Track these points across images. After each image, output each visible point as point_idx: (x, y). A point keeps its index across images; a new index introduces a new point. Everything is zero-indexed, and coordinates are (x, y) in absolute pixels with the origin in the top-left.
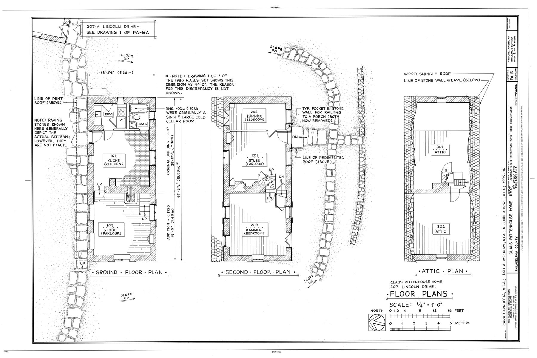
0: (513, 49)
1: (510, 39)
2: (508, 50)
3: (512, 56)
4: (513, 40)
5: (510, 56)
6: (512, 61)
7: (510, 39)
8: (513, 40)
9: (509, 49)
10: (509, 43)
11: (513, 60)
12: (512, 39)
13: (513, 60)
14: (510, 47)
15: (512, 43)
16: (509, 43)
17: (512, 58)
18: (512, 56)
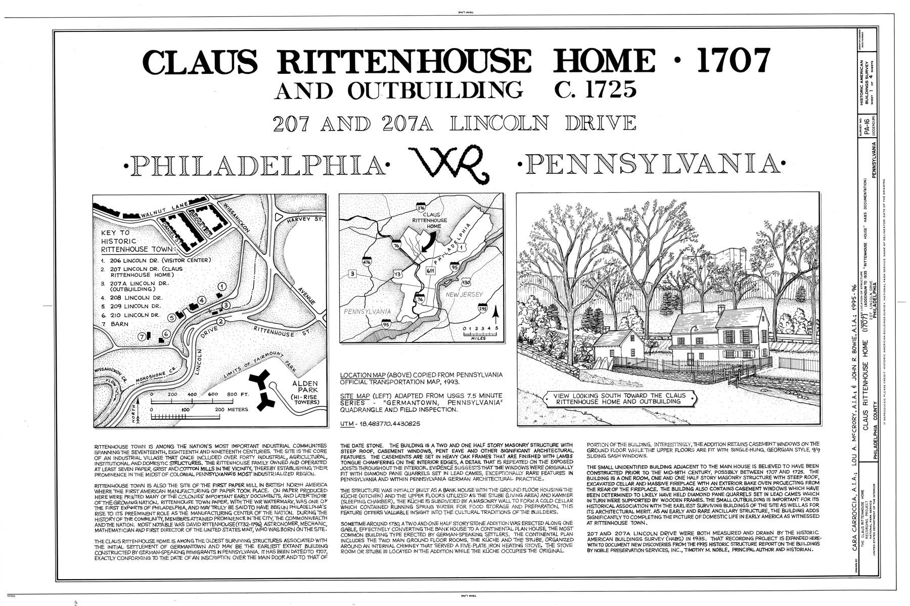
0: (869, 83)
1: (864, 65)
2: (860, 84)
3: (136, 289)
4: (870, 67)
5: (864, 95)
6: (867, 103)
7: (864, 65)
8: (870, 67)
9: (861, 82)
10: (861, 73)
11: (870, 101)
12: (867, 66)
13: (870, 101)
14: (864, 80)
15: (867, 72)
16: (861, 73)
17: (867, 97)
18: (136, 289)
